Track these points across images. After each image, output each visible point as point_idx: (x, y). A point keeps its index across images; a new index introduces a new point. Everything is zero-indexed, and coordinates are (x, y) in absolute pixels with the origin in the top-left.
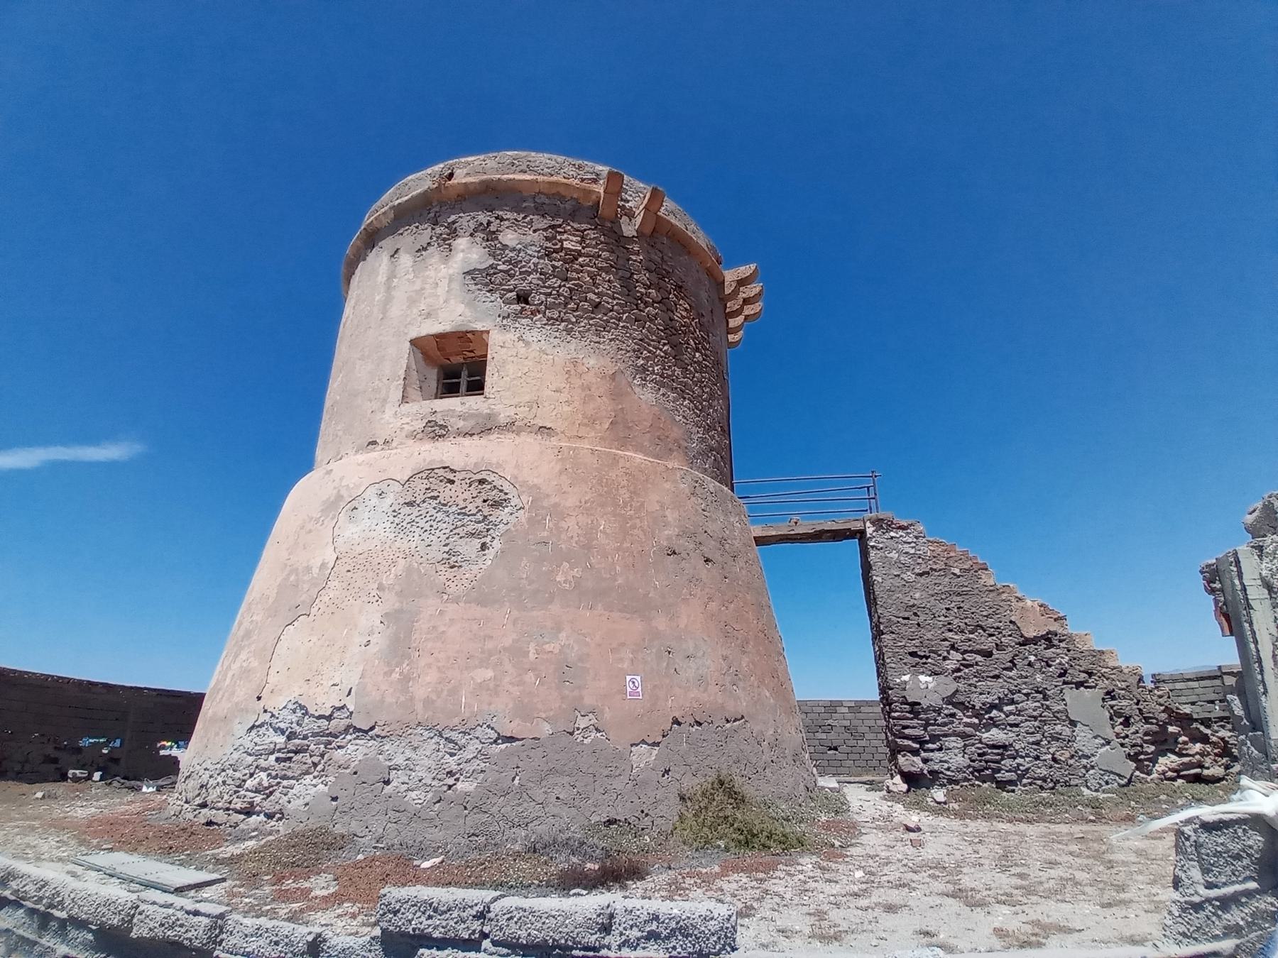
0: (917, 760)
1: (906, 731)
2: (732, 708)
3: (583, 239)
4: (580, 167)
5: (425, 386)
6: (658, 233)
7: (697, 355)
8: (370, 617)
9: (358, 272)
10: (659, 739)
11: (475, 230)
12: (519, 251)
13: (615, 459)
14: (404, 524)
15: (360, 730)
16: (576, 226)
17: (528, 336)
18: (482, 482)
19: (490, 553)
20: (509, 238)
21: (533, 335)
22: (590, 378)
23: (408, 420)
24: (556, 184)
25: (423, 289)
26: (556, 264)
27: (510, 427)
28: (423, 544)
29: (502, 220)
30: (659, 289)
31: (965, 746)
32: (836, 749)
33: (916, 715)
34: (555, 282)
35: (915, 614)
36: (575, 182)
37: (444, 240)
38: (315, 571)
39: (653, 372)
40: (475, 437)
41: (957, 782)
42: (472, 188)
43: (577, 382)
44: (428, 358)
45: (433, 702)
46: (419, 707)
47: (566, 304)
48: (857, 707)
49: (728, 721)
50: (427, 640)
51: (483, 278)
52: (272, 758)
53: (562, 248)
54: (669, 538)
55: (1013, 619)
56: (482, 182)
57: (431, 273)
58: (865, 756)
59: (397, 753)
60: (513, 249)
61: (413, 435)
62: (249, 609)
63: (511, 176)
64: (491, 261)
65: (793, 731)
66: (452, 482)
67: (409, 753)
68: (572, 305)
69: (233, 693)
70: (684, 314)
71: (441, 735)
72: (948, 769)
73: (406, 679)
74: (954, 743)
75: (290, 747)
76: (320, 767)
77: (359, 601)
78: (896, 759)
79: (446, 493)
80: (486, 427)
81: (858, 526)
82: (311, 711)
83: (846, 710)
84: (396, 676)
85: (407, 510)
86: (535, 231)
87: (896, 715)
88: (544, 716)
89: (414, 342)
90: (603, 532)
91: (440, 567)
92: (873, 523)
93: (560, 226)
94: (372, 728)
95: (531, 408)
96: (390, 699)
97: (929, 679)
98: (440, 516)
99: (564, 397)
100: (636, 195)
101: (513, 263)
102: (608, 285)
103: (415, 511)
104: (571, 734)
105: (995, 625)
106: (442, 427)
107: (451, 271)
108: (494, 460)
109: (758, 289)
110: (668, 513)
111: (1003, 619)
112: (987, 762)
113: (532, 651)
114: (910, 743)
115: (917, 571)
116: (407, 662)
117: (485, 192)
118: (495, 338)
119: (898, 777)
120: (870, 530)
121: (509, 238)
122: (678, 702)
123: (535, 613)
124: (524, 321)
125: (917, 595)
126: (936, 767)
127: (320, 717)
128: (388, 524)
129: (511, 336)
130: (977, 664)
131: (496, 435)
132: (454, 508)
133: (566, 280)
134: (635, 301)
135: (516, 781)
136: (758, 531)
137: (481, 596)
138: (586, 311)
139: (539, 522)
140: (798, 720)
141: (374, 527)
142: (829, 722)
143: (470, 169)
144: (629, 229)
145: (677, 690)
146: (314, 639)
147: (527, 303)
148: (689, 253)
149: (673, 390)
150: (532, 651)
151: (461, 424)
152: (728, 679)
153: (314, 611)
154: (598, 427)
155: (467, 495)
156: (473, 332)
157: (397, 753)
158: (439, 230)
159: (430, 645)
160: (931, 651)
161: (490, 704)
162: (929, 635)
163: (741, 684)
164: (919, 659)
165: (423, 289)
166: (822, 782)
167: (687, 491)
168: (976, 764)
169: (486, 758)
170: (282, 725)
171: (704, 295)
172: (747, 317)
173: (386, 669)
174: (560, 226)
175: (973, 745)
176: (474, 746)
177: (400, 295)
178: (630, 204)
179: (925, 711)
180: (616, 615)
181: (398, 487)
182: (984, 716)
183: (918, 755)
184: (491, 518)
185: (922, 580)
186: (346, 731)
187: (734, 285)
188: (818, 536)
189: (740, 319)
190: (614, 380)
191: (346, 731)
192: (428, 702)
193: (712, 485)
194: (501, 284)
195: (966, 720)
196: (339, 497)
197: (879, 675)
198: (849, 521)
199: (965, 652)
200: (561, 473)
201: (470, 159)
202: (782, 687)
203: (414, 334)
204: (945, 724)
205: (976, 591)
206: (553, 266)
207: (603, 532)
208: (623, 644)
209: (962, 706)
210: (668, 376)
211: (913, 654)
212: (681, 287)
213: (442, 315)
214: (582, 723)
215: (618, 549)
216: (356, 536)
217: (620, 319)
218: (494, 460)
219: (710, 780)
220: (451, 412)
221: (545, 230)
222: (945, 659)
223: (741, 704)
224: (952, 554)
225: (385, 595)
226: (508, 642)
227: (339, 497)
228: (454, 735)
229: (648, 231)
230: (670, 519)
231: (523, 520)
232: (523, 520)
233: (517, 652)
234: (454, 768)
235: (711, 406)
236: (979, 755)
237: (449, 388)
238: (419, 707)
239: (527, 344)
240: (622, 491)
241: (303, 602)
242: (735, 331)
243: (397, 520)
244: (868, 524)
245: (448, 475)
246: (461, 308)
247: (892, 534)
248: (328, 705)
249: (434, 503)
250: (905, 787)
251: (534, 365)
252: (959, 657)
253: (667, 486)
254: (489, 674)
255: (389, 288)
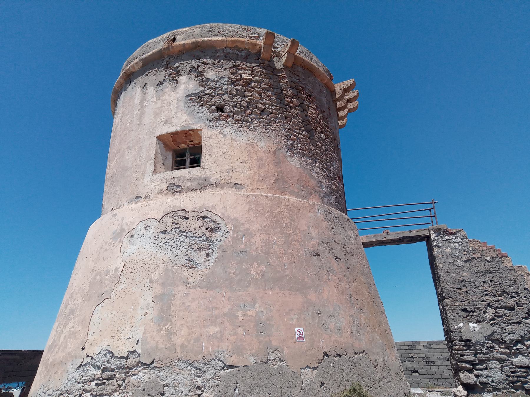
0: (471, 375)
1: (464, 358)
2: (359, 345)
3: (253, 72)
4: (248, 30)
5: (166, 162)
6: (296, 66)
7: (322, 135)
8: (146, 298)
9: (122, 97)
10: (317, 365)
11: (190, 71)
12: (217, 82)
13: (280, 200)
14: (161, 244)
15: (145, 364)
16: (248, 64)
17: (224, 131)
18: (204, 217)
19: (212, 259)
20: (210, 74)
21: (228, 131)
22: (262, 154)
23: (158, 183)
24: (236, 41)
25: (162, 107)
26: (238, 88)
27: (217, 184)
28: (172, 255)
29: (206, 64)
30: (298, 98)
31: (502, 367)
32: (417, 372)
33: (469, 348)
34: (238, 98)
35: (464, 286)
36: (247, 39)
37: (173, 77)
38: (112, 273)
39: (298, 148)
40: (198, 192)
41: (498, 390)
42: (187, 46)
43: (255, 156)
44: (166, 146)
45: (186, 346)
46: (178, 350)
47: (245, 111)
48: (429, 345)
49: (356, 354)
50: (180, 311)
51: (197, 99)
52: (93, 384)
53: (241, 78)
54: (313, 246)
55: (526, 286)
56: (193, 43)
57: (167, 97)
58: (436, 376)
59: (167, 377)
60: (213, 81)
61: (161, 192)
62: (71, 297)
63: (210, 39)
64: (201, 89)
65: (394, 359)
66: (187, 218)
67: (174, 376)
68: (248, 112)
69: (66, 347)
70: (313, 111)
71: (192, 366)
72: (493, 381)
73: (170, 334)
74: (494, 364)
75: (104, 376)
76: (122, 388)
77: (139, 290)
78: (458, 375)
79: (184, 225)
80: (204, 185)
81: (426, 233)
82: (116, 354)
83: (422, 347)
84: (164, 332)
85: (162, 236)
86: (225, 69)
87: (456, 347)
88: (249, 352)
89: (159, 138)
90: (276, 244)
91: (184, 268)
92: (435, 231)
93: (239, 65)
94: (152, 363)
95: (229, 173)
96: (161, 346)
97: (475, 325)
98: (181, 238)
99: (248, 165)
100: (282, 45)
101: (214, 89)
102: (269, 97)
103: (167, 236)
104: (266, 363)
105: (515, 291)
106: (179, 186)
107: (178, 96)
108: (210, 205)
109: (355, 94)
110: (312, 231)
111: (520, 287)
112: (517, 377)
113: (240, 315)
114: (466, 365)
115: (464, 259)
116: (169, 324)
117: (195, 48)
118: (206, 133)
119: (461, 386)
120: (433, 235)
121: (210, 74)
122: (327, 342)
123: (240, 293)
124: (222, 122)
125: (465, 274)
126: (485, 380)
127: (121, 358)
128: (152, 245)
129: (215, 132)
130: (505, 315)
131: (210, 190)
132: (189, 234)
133: (244, 97)
134: (284, 106)
135: (237, 391)
136: (364, 239)
137: (209, 284)
138: (257, 114)
139: (239, 239)
140: (396, 353)
141: (144, 246)
142: (412, 355)
143: (185, 36)
144: (279, 64)
145: (325, 336)
146: (114, 313)
147: (223, 112)
148: (314, 75)
149: (310, 157)
150: (240, 315)
151: (189, 184)
152: (354, 328)
153: (113, 296)
154: (268, 182)
155: (196, 226)
156: (193, 130)
157: (167, 377)
158: (169, 72)
159: (182, 313)
160: (476, 308)
161: (218, 347)
162: (473, 298)
163: (362, 331)
164: (469, 313)
165: (162, 107)
166: (413, 390)
167: (322, 217)
168: (511, 379)
169: (219, 378)
170: (99, 364)
171: (324, 99)
172: (349, 110)
173: (158, 328)
174: (239, 65)
175: (507, 366)
176: (212, 371)
177: (149, 111)
178: (278, 50)
179: (475, 345)
180: (286, 292)
181: (156, 223)
182: (513, 347)
183: (473, 373)
184: (211, 239)
185: (467, 265)
186: (137, 365)
187: (341, 92)
188: (401, 241)
189: (345, 112)
190: (275, 154)
191: (137, 365)
192: (183, 347)
193: (336, 213)
194: (207, 102)
195: (501, 350)
196: (122, 230)
197: (444, 323)
198: (420, 231)
199: (496, 308)
200: (249, 210)
201: (185, 29)
202: (386, 334)
203: (159, 133)
204: (487, 353)
205: (501, 270)
206: (236, 89)
207: (276, 244)
208: (292, 310)
209: (498, 342)
210: (306, 150)
211: (464, 310)
212: (310, 96)
213: (174, 121)
214: (272, 356)
215: (285, 254)
216: (134, 252)
217: (276, 118)
218: (210, 205)
219: (348, 388)
220: (182, 178)
221: (231, 68)
222: (484, 312)
223: (362, 343)
224: (485, 248)
225: (154, 286)
226: (226, 310)
227: (122, 230)
228: (199, 365)
229: (290, 64)
230: (313, 234)
231: (230, 239)
232: (230, 239)
233: (232, 316)
234: (201, 384)
235: (332, 166)
236: (512, 372)
237: (179, 164)
238: (178, 350)
239: (225, 136)
240: (285, 219)
241: (106, 291)
242: (342, 118)
243: (157, 242)
244: (432, 232)
245: (184, 214)
246: (185, 117)
247: (447, 237)
248: (126, 350)
249: (177, 231)
250: (465, 393)
251: (226, 146)
252: (493, 311)
253: (311, 215)
254: (217, 329)
255: (142, 107)
